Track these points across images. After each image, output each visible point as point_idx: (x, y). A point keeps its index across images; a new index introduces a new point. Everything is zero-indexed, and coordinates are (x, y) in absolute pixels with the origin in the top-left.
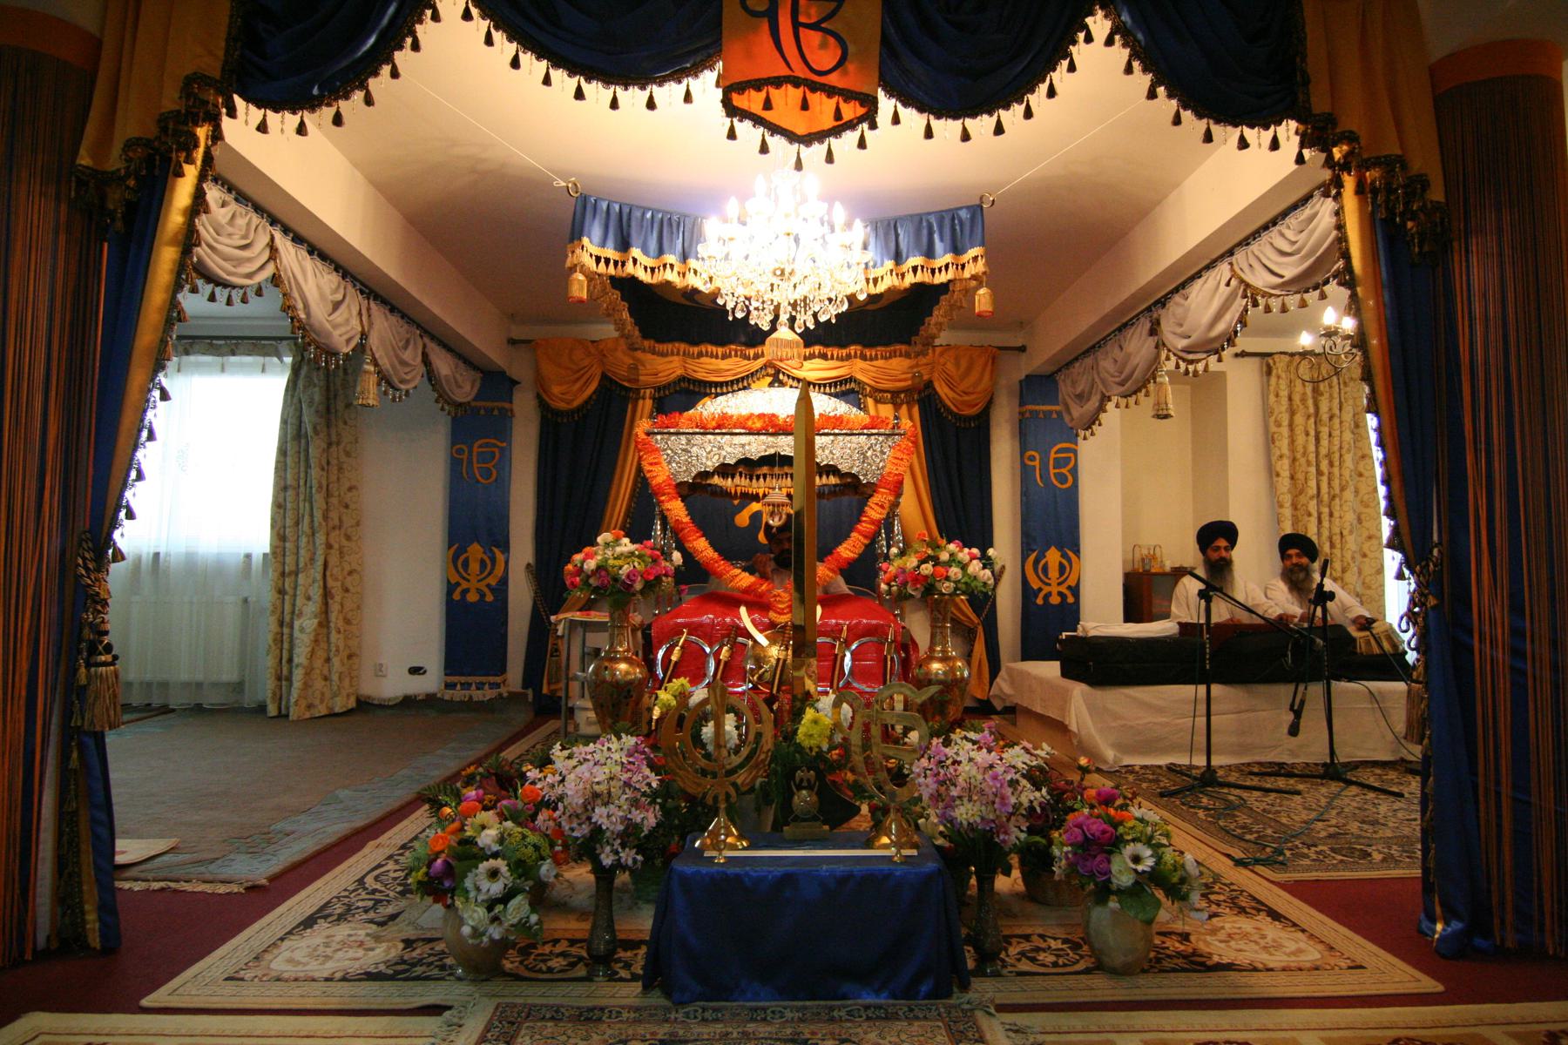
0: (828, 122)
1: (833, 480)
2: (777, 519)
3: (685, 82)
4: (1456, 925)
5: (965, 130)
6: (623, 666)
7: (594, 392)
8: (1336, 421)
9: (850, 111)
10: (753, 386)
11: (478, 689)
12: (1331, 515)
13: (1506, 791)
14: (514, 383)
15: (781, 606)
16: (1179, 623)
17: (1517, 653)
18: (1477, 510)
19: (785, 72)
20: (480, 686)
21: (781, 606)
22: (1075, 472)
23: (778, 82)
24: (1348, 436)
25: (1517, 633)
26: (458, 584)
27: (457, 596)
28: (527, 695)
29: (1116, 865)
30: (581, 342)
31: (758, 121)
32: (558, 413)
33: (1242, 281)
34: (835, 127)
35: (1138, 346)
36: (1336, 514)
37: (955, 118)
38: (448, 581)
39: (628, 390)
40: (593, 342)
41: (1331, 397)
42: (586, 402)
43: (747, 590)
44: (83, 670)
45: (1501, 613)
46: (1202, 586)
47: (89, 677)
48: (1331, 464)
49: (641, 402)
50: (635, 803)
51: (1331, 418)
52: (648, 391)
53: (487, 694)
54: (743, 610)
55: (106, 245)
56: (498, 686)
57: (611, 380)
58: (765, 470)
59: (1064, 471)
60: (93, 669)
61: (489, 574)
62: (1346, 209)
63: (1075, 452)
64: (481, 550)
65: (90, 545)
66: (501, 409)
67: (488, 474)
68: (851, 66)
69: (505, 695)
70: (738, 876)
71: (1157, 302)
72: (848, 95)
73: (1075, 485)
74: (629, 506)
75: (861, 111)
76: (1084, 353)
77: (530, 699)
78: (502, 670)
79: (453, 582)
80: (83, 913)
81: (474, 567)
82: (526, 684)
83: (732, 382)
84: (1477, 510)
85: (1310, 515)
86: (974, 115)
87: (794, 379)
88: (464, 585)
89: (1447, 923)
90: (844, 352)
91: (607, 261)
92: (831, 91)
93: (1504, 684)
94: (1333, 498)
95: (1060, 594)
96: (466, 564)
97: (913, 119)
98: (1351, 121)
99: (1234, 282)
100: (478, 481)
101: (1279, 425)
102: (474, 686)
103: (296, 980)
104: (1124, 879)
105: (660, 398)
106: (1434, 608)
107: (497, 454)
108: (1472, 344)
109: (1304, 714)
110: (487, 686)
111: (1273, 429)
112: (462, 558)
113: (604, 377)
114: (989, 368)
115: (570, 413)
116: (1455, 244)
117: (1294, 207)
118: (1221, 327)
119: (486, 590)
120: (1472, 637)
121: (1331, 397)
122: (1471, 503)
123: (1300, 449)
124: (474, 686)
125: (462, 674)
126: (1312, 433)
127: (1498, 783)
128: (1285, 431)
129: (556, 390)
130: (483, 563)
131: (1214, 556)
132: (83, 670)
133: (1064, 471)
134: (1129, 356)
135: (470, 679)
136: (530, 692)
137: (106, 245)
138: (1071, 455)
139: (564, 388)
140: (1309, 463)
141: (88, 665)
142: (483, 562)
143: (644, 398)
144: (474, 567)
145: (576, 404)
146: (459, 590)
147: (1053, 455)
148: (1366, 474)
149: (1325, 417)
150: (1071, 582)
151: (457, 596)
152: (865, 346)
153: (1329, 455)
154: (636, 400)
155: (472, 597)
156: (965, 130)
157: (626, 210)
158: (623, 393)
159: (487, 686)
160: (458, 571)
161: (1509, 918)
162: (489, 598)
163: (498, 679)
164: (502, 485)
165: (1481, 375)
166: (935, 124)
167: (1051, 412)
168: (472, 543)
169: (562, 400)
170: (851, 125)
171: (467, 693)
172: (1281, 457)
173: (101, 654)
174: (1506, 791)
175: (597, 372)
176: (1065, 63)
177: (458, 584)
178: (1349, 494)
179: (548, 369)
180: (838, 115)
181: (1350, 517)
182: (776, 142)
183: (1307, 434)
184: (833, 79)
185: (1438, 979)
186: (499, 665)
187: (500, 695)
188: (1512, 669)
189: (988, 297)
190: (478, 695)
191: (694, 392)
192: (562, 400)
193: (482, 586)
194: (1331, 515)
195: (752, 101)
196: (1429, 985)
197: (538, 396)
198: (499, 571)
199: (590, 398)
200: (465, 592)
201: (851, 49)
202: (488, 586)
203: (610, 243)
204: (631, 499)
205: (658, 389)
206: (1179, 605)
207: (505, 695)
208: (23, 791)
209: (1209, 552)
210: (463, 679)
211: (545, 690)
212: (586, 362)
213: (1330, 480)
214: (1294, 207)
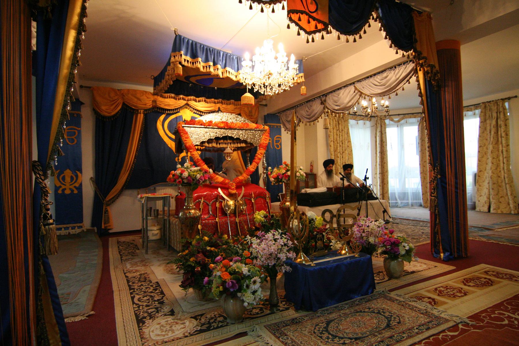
0: (313, 29)
1: (243, 145)
2: (229, 158)
3: (272, 5)
4: (447, 254)
5: (347, 39)
6: (193, 211)
7: (120, 110)
8: (343, 131)
9: (320, 26)
10: (181, 111)
11: (72, 229)
12: (343, 157)
13: (454, 220)
14: (82, 103)
15: (233, 187)
16: (327, 188)
17: (456, 188)
18: (447, 155)
19: (303, 9)
20: (73, 228)
21: (233, 187)
22: (281, 144)
23: (302, 12)
24: (346, 136)
25: (456, 183)
26: (60, 187)
27: (60, 192)
28: (94, 230)
29: (401, 248)
30: (114, 90)
31: (297, 24)
32: (104, 117)
33: (359, 91)
34: (314, 31)
35: (317, 107)
36: (344, 157)
37: (345, 35)
38: (56, 186)
39: (133, 109)
40: (118, 90)
41: (342, 125)
42: (117, 113)
43: (222, 183)
44: (43, 227)
45: (453, 180)
46: (342, 177)
47: (46, 230)
48: (342, 144)
49: (139, 115)
50: (288, 251)
51: (342, 131)
52: (142, 111)
53: (77, 231)
54: (220, 190)
55: (34, 24)
56: (81, 227)
57: (127, 106)
58: (222, 141)
59: (278, 144)
60: (47, 227)
61: (75, 182)
62: (419, 76)
63: (281, 138)
64: (71, 172)
65: (41, 168)
66: (77, 115)
67: (73, 140)
68: (319, 12)
69: (85, 230)
70: (325, 268)
71: (324, 95)
72: (319, 21)
73: (281, 148)
74: (136, 154)
75: (323, 27)
76: (291, 108)
77: (96, 231)
78: (81, 221)
79: (58, 186)
80: (48, 340)
81: (68, 179)
82: (93, 224)
83: (174, 109)
84: (447, 155)
85: (338, 157)
86: (350, 35)
87: (195, 110)
88: (63, 187)
89: (444, 253)
90: (216, 100)
91: (188, 61)
92: (314, 19)
93: (454, 195)
94: (343, 153)
95: (70, 189)
96: (64, 179)
97: (335, 33)
98: (425, 54)
99: (356, 92)
100: (68, 144)
101: (331, 132)
102: (70, 228)
103: (173, 340)
104: (403, 252)
105: (146, 114)
106: (440, 178)
107: (77, 133)
108: (446, 112)
109: (361, 211)
110: (76, 228)
111: (329, 133)
112: (62, 176)
113: (124, 104)
114: (257, 112)
115: (109, 118)
116: (442, 89)
117: (379, 73)
118: (350, 104)
119: (75, 189)
120: (446, 185)
121: (342, 125)
122: (446, 154)
123: (335, 139)
124: (70, 228)
125: (64, 224)
126: (338, 134)
127: (453, 219)
128: (332, 134)
129: (103, 108)
130: (72, 178)
131: (329, 169)
132: (43, 227)
133: (278, 144)
134: (313, 110)
135: (68, 226)
136: (95, 228)
137: (34, 24)
138: (280, 139)
139: (107, 107)
140: (338, 143)
141: (45, 225)
142: (72, 177)
143: (140, 113)
144: (68, 179)
145: (113, 113)
146: (61, 189)
147: (275, 139)
148: (350, 146)
149: (341, 130)
150: (77, 185)
151: (60, 192)
152: (215, 99)
153: (342, 141)
154: (138, 113)
155: (67, 192)
156: (347, 39)
157: (194, 44)
158: (132, 111)
159: (76, 228)
160: (60, 182)
161: (455, 250)
162: (76, 192)
163: (81, 224)
164: (78, 145)
165: (448, 121)
166: (341, 36)
167: (274, 125)
168: (66, 169)
169: (106, 112)
170: (319, 31)
171: (67, 231)
172: (331, 141)
173: (49, 219)
174: (454, 220)
175: (120, 101)
176: (368, 24)
177: (60, 187)
178: (346, 152)
179: (98, 99)
180: (316, 27)
181: (347, 158)
182: (302, 32)
183: (337, 135)
184: (314, 15)
185: (455, 266)
186: (80, 219)
187: (83, 231)
188: (455, 192)
189: (305, 89)
190: (72, 232)
191: (159, 112)
192: (106, 112)
193: (72, 187)
194: (343, 157)
195: (295, 17)
196: (452, 268)
197: (94, 110)
198: (79, 181)
199: (118, 112)
200: (64, 190)
201: (319, 6)
202: (75, 187)
203: (189, 54)
204: (136, 152)
205: (146, 110)
206: (319, 182)
207: (85, 230)
208: (26, 288)
209: (328, 167)
210: (65, 226)
211: (103, 227)
212: (116, 98)
213: (342, 148)
214: (379, 73)
